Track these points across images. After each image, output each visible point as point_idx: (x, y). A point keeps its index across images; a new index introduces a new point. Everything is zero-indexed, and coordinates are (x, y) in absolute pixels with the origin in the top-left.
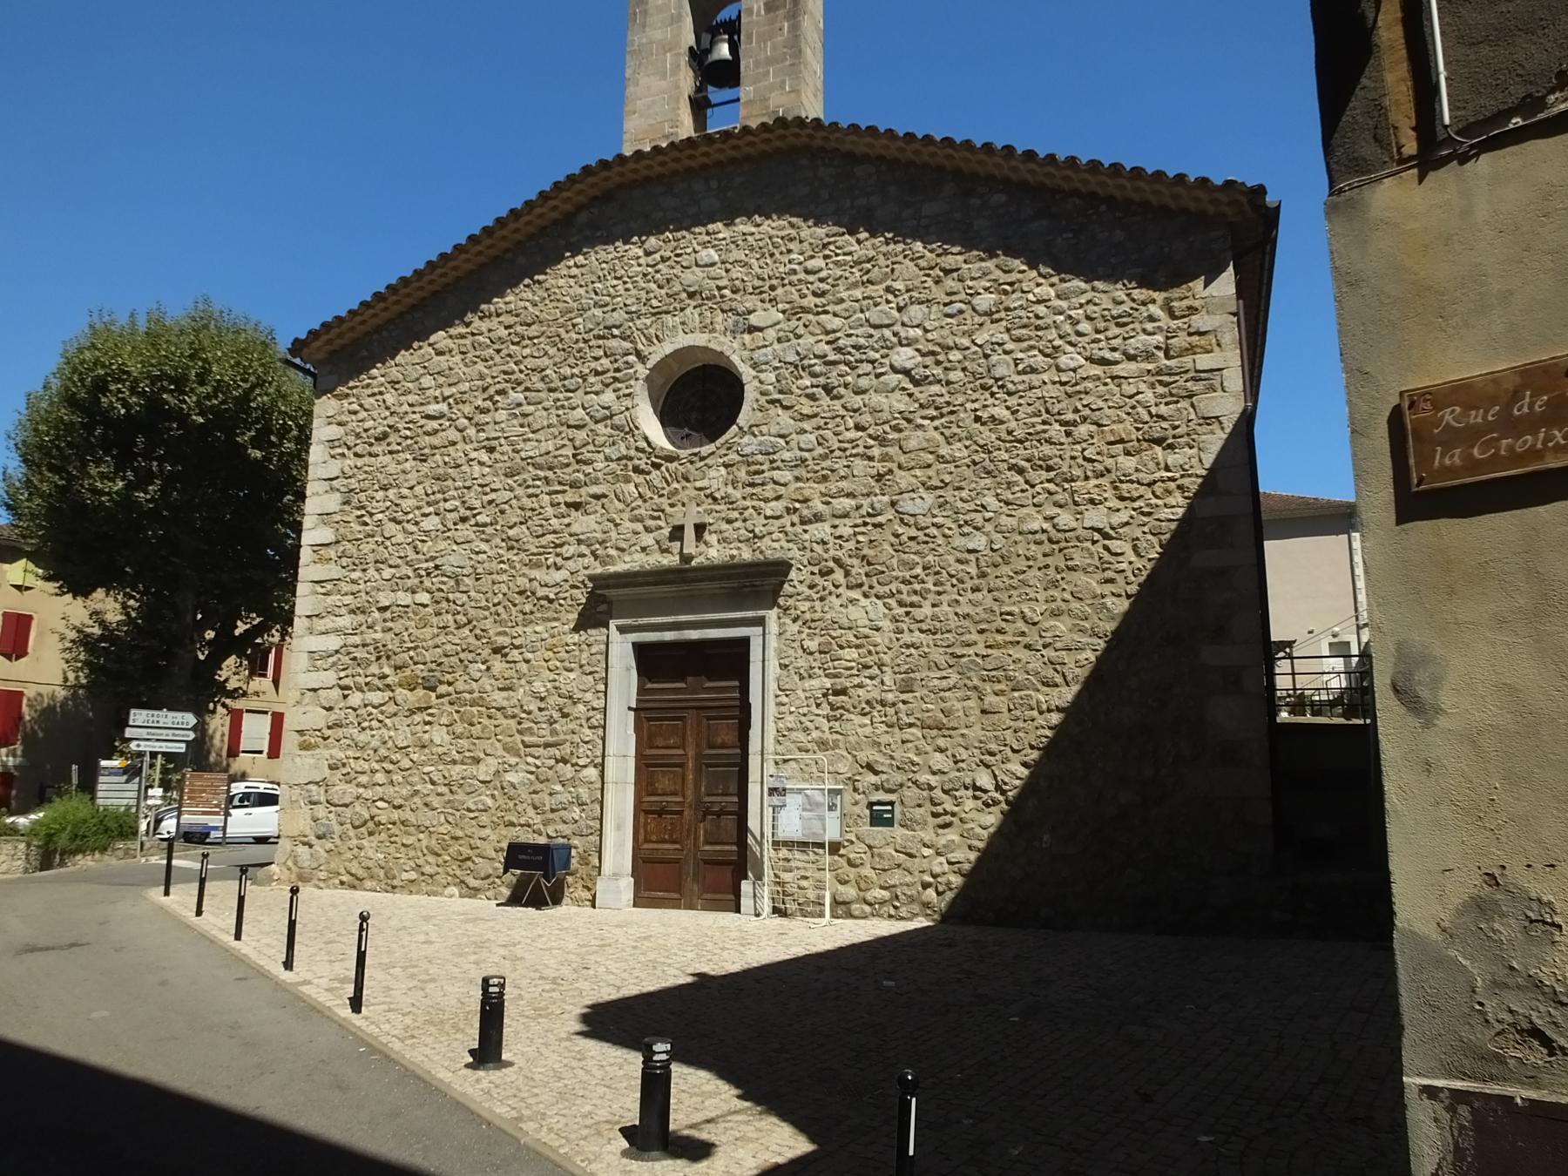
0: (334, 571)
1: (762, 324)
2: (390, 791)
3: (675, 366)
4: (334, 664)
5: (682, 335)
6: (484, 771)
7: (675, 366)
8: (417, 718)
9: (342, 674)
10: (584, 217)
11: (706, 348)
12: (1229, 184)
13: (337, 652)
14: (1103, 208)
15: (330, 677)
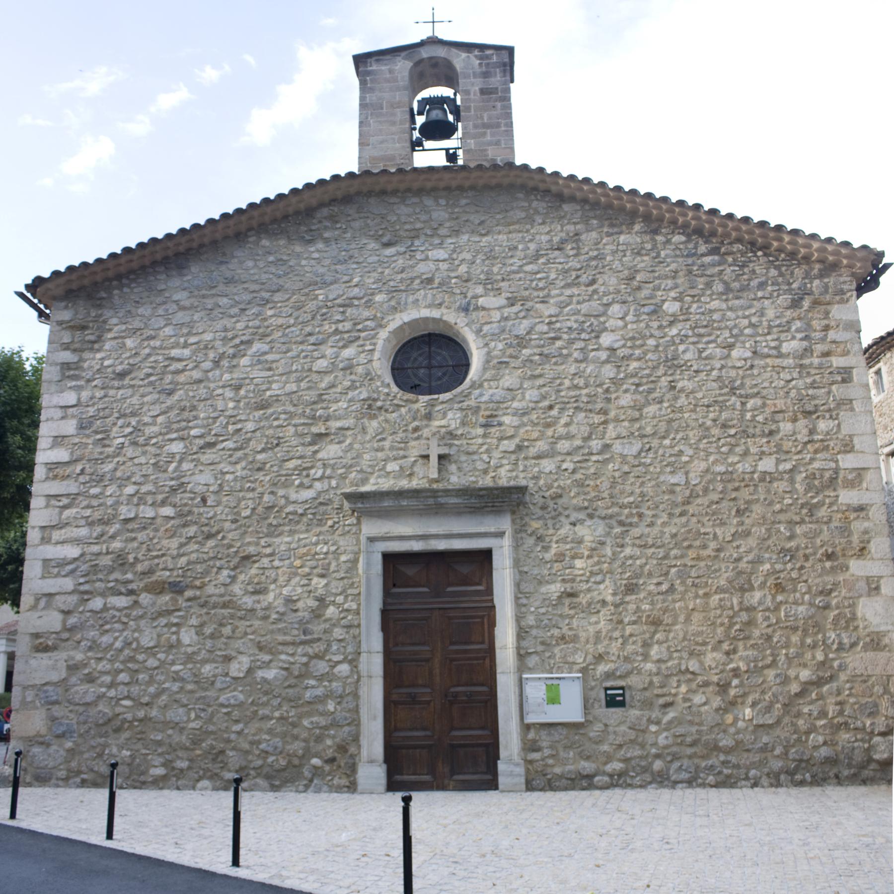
0: (71, 487)
1: (487, 306)
2: (135, 690)
3: (441, 325)
4: (73, 571)
5: (418, 311)
6: (237, 668)
7: (441, 325)
8: (163, 621)
9: (82, 580)
10: (325, 211)
11: (441, 320)
12: (865, 247)
13: (75, 559)
14: (760, 253)
15: (68, 584)
